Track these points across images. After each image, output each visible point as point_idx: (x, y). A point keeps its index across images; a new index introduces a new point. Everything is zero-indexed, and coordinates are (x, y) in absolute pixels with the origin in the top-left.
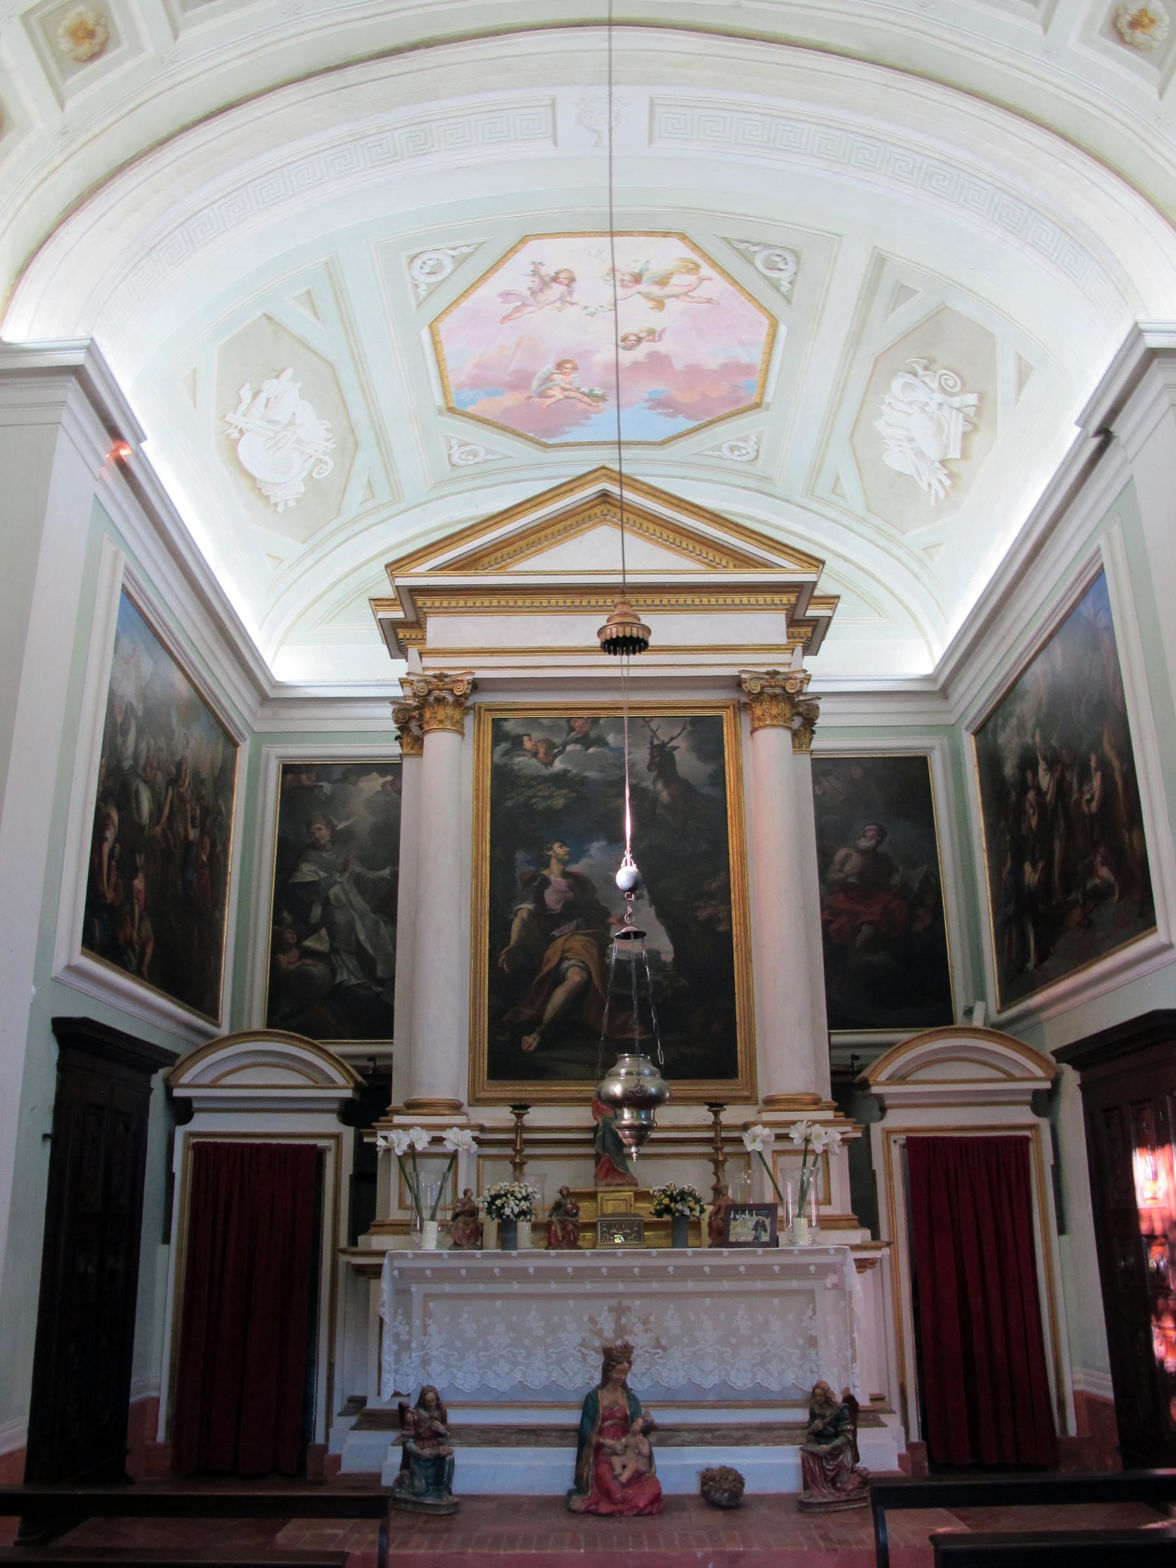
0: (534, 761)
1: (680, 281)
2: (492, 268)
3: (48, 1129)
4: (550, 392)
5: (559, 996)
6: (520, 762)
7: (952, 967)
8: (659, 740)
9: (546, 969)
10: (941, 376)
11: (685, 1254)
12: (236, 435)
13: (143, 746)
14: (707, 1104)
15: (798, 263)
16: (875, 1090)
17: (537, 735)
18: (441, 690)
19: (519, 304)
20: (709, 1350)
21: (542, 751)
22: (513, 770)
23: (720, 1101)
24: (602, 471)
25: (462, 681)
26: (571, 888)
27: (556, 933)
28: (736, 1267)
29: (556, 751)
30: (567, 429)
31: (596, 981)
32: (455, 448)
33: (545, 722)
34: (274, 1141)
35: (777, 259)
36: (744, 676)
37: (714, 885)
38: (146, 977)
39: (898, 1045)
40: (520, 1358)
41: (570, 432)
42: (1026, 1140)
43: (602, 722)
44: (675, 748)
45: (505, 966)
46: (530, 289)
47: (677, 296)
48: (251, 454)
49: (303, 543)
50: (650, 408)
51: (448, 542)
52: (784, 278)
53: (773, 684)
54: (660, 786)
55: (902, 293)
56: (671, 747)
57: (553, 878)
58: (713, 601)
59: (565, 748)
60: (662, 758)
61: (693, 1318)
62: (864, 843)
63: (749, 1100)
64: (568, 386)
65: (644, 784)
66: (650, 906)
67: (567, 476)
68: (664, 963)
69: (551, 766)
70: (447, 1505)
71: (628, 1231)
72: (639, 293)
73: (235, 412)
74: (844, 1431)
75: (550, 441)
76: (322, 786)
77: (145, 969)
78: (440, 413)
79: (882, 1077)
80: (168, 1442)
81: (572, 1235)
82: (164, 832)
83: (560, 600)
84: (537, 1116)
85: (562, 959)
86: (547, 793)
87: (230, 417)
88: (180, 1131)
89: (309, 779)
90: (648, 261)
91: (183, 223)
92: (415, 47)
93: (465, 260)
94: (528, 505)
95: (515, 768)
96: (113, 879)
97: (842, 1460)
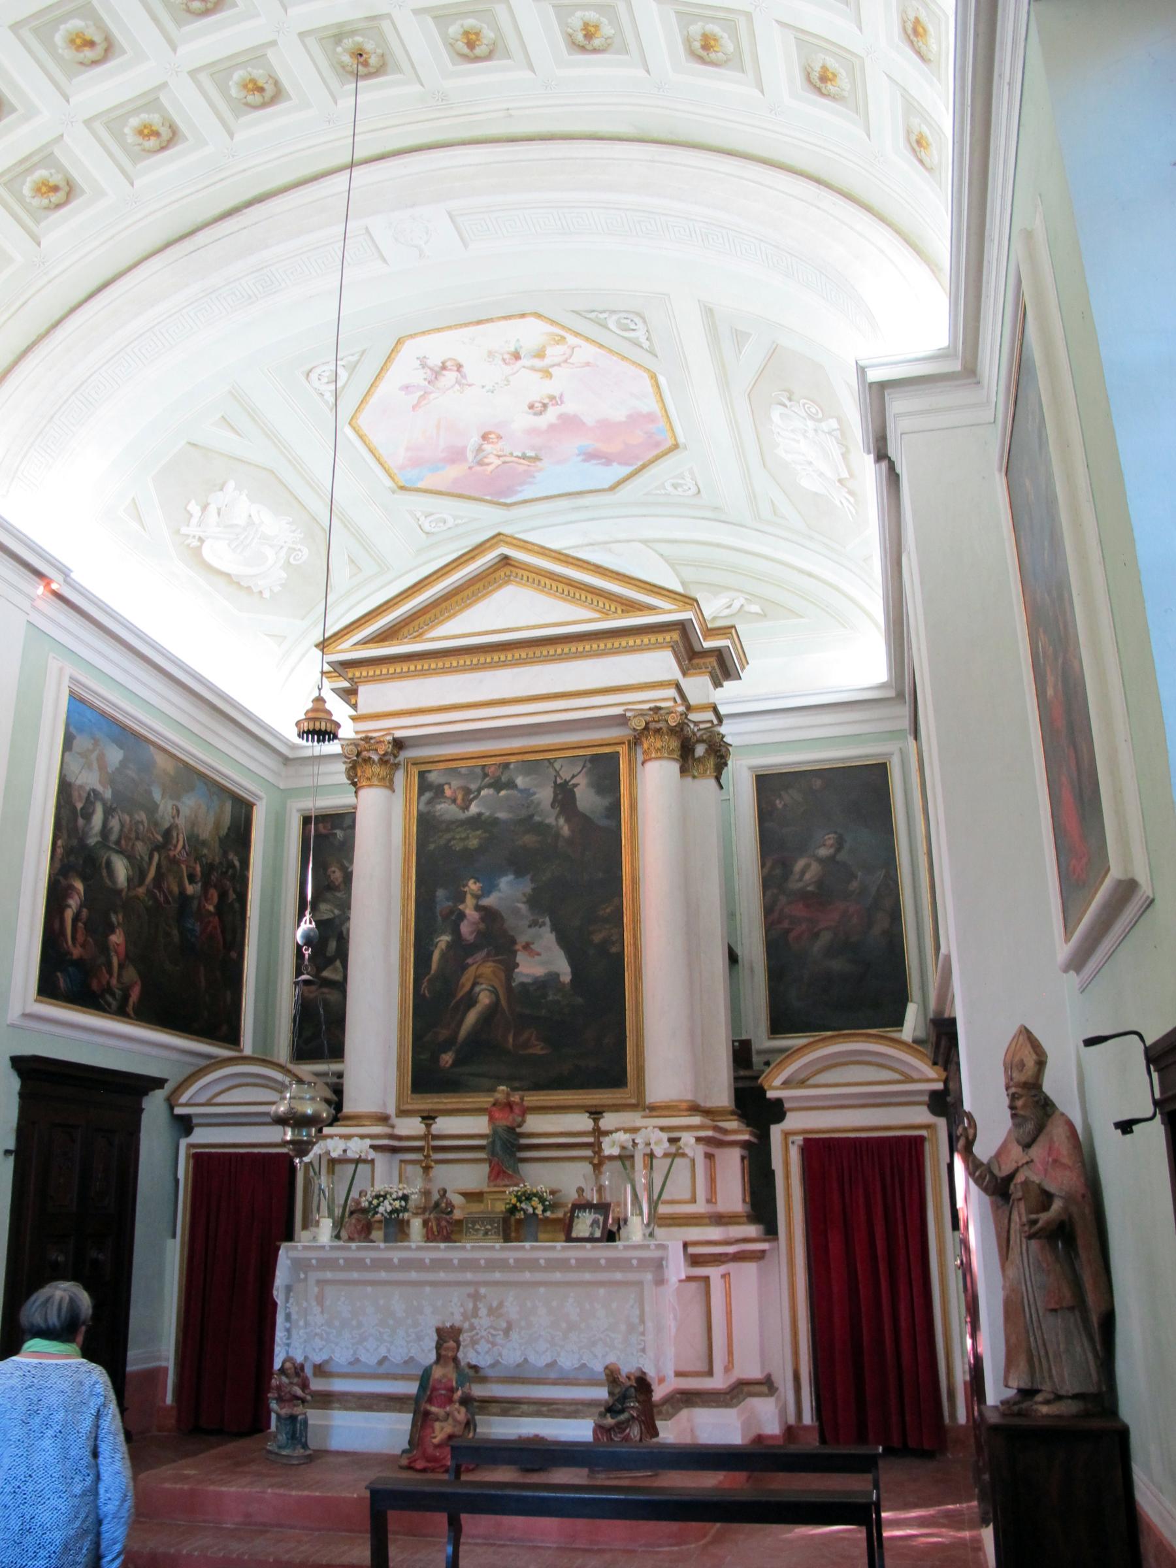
0: (453, 807)
1: (555, 353)
2: (382, 368)
3: (11, 1144)
4: (486, 461)
5: (472, 1017)
6: (441, 808)
7: (909, 968)
8: (561, 778)
9: (461, 994)
10: (804, 405)
11: (523, 1247)
12: (196, 543)
13: (114, 823)
14: (587, 1112)
15: (645, 322)
16: (771, 1094)
17: (455, 783)
18: (368, 751)
19: (422, 393)
20: (484, 1333)
21: (460, 797)
22: (434, 816)
23: (599, 1110)
24: (498, 538)
25: (384, 742)
26: (483, 919)
27: (470, 961)
28: (567, 1260)
29: (472, 796)
30: (519, 489)
31: (503, 1002)
32: (422, 519)
33: (463, 771)
34: (256, 1150)
35: (625, 321)
36: (628, 714)
37: (608, 910)
38: (132, 1015)
39: (792, 1051)
40: (385, 1337)
41: (523, 490)
42: (920, 1140)
43: (512, 766)
44: (576, 785)
45: (426, 992)
46: (425, 379)
47: (559, 365)
48: (218, 553)
49: (303, 619)
50: (585, 461)
51: (367, 618)
52: (640, 335)
53: (656, 719)
54: (562, 821)
55: (740, 337)
56: (573, 784)
57: (468, 912)
58: (602, 646)
59: (479, 793)
60: (564, 795)
61: (587, 1306)
62: (823, 852)
63: (634, 1107)
64: (500, 453)
65: (547, 821)
66: (551, 932)
67: (467, 547)
68: (563, 984)
69: (468, 811)
70: (297, 1457)
71: (489, 1227)
72: (524, 367)
73: (188, 525)
74: (628, 1407)
75: (509, 501)
76: (336, 834)
77: (130, 1009)
78: (394, 492)
79: (777, 1082)
80: (174, 1404)
81: (445, 1231)
82: (149, 893)
83: (467, 660)
84: (443, 1125)
85: (475, 984)
86: (463, 835)
87: (184, 530)
88: (183, 1143)
89: (324, 827)
90: (518, 340)
91: (77, 390)
92: (249, 204)
93: (355, 366)
94: (435, 577)
95: (437, 814)
96: (80, 937)
97: (629, 1434)
